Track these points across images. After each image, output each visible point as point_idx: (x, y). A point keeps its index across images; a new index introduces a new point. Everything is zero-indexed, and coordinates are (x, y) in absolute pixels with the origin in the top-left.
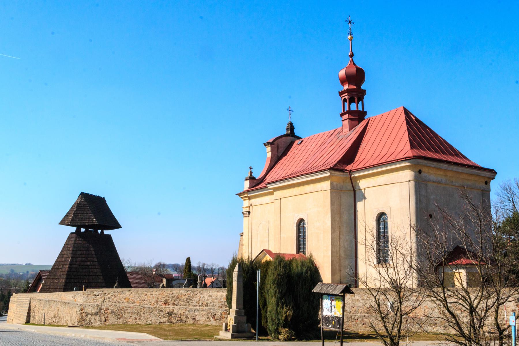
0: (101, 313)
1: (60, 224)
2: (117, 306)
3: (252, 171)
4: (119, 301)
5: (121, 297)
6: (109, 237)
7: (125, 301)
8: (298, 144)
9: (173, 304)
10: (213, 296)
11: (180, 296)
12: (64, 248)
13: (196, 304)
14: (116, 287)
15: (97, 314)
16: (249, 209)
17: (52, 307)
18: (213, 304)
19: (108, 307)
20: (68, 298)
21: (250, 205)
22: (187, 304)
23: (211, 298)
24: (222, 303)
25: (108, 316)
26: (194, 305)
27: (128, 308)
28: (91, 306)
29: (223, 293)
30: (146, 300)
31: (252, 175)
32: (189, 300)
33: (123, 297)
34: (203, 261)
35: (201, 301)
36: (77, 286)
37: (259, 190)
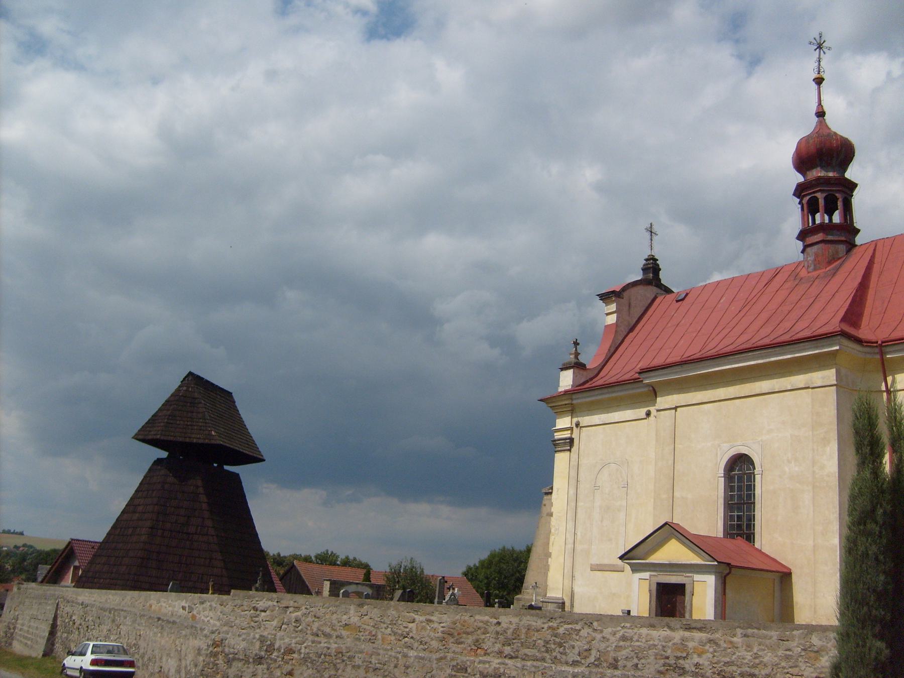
0: (271, 659)
1: (132, 438)
2: (322, 645)
3: (579, 351)
4: (328, 630)
5: (335, 622)
6: (236, 477)
7: (344, 633)
8: (677, 301)
9: (500, 653)
10: (636, 638)
11: (524, 631)
12: (137, 491)
13: (579, 658)
14: (257, 590)
15: (259, 660)
16: (572, 434)
17: (121, 627)
18: (635, 661)
19: (293, 645)
20: (170, 609)
21: (574, 426)
22: (548, 656)
23: (628, 643)
24: (667, 661)
25: (293, 670)
26: (570, 661)
27: (356, 652)
28: (244, 636)
29: (668, 632)
30: (411, 635)
31: (578, 359)
32: (553, 646)
33: (339, 622)
34: (269, 551)
35: (594, 653)
36: (176, 580)
37: (606, 390)
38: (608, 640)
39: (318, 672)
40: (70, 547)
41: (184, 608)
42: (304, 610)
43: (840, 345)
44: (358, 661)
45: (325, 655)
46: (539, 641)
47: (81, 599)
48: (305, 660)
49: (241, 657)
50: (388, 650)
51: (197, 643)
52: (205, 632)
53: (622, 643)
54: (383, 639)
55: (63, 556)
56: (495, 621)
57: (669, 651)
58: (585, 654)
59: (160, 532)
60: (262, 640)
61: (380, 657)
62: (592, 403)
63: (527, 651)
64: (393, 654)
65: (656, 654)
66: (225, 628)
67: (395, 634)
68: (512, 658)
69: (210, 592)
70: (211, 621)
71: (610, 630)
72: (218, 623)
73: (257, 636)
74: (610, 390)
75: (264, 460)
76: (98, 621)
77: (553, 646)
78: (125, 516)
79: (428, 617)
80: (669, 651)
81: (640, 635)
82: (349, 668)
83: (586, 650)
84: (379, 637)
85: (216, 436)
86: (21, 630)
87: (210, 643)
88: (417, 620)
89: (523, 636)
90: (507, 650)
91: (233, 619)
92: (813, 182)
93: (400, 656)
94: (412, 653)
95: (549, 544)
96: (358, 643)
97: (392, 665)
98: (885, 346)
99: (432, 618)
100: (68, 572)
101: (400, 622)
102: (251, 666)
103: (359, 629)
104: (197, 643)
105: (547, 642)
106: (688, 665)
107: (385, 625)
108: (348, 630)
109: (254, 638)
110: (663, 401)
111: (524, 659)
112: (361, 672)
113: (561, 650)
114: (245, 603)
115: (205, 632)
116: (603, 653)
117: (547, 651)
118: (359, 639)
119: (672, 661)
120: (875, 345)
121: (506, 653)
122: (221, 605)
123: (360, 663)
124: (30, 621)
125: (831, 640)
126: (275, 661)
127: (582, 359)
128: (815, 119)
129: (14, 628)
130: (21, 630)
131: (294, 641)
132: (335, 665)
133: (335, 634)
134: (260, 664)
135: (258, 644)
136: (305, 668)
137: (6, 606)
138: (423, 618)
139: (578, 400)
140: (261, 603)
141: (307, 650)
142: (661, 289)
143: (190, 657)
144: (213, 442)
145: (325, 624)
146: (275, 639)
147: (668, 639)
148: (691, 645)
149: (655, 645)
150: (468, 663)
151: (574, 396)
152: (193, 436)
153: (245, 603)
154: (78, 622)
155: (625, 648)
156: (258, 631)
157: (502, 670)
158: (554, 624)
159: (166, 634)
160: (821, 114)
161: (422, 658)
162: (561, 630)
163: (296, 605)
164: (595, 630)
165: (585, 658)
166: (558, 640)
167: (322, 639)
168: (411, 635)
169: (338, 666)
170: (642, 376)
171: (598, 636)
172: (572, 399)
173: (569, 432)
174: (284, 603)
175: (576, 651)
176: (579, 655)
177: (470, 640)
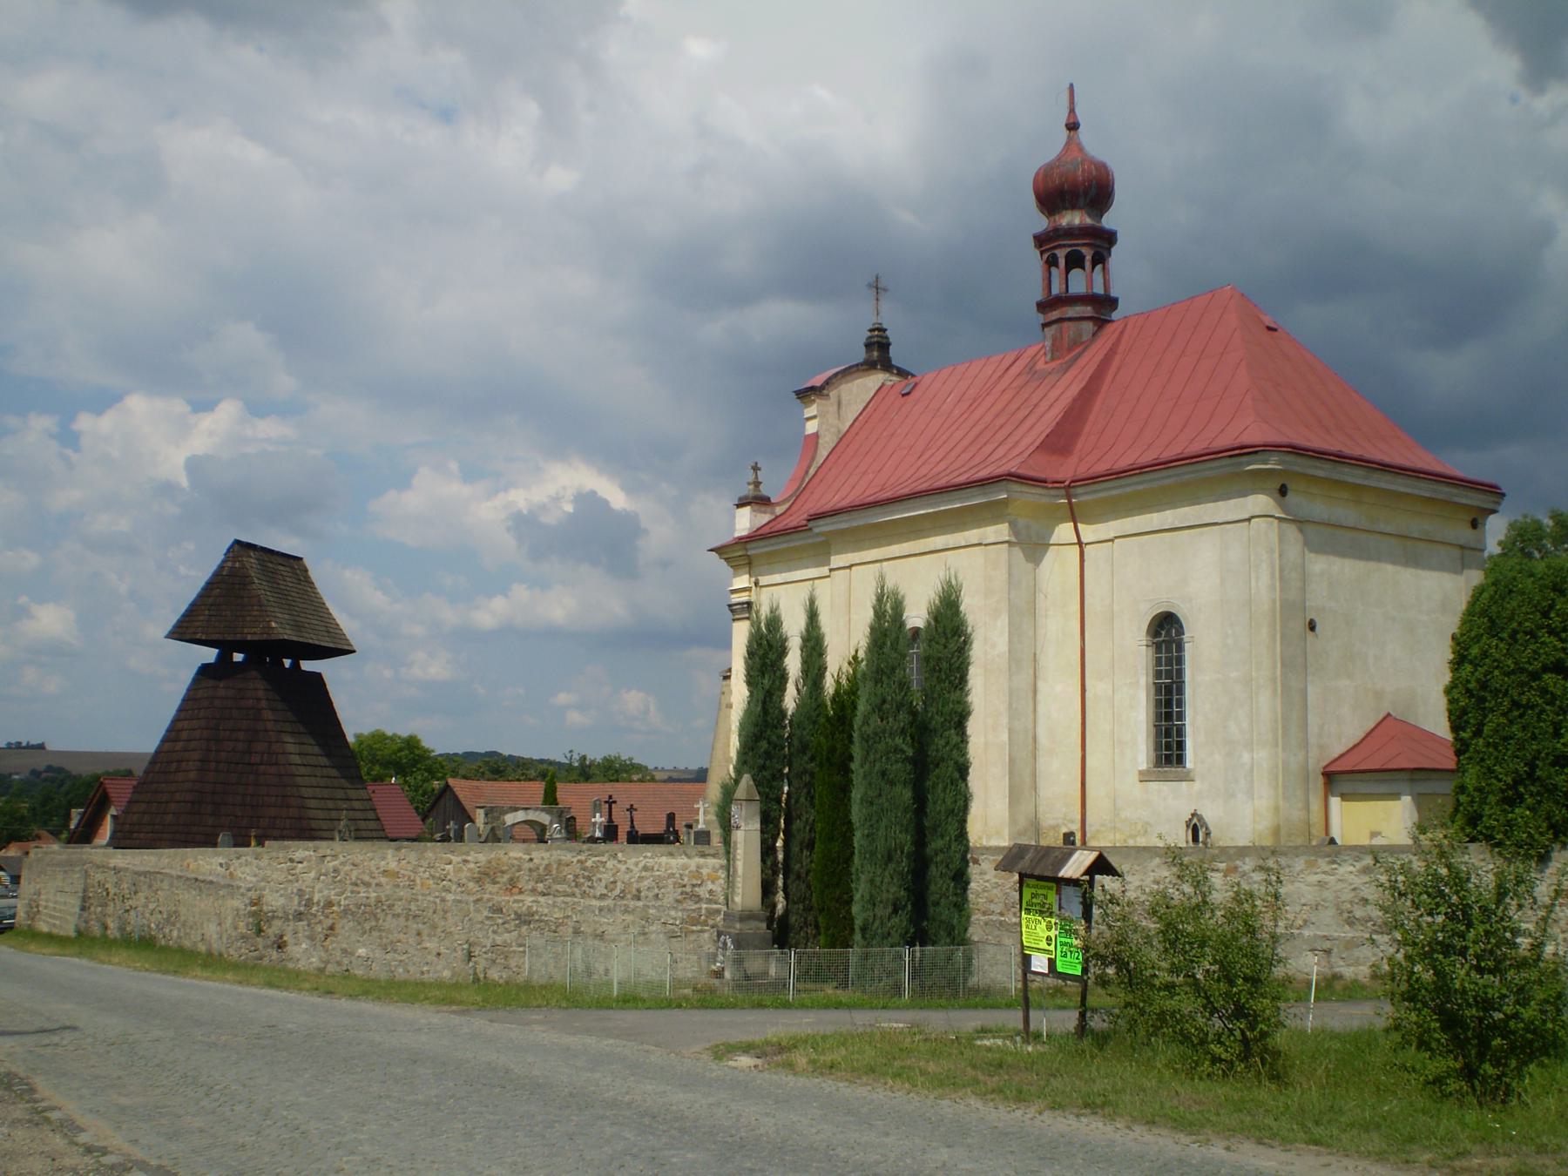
0: (312, 914)
2: (362, 895)
4: (366, 878)
5: (373, 869)
6: (317, 678)
7: (383, 880)
8: (903, 395)
9: (534, 890)
11: (555, 866)
13: (605, 892)
15: (299, 916)
17: (159, 892)
18: (656, 891)
23: (648, 874)
25: (334, 924)
28: (282, 892)
29: (684, 860)
30: (449, 877)
32: (582, 880)
33: (378, 868)
38: (632, 871)
39: (359, 924)
40: (100, 791)
41: (221, 865)
42: (341, 858)
43: (1007, 491)
44: (398, 910)
45: (365, 906)
46: (569, 876)
47: (113, 862)
48: (346, 911)
49: (280, 915)
50: (426, 895)
51: (237, 903)
52: (242, 890)
53: (644, 874)
54: (422, 884)
55: (94, 802)
56: (527, 857)
57: (686, 879)
58: (612, 886)
59: (213, 765)
60: (301, 893)
61: (419, 903)
62: (770, 554)
63: (559, 887)
64: (432, 899)
65: (675, 883)
66: (263, 884)
67: (433, 877)
68: (544, 895)
69: (253, 843)
70: (248, 878)
71: (633, 860)
72: (254, 879)
73: (295, 891)
74: (788, 538)
75: (354, 651)
76: (133, 888)
77: (582, 880)
78: (167, 746)
79: (464, 857)
80: (686, 879)
81: (660, 865)
82: (390, 917)
83: (612, 882)
84: (418, 881)
85: (281, 628)
86: (46, 907)
87: (247, 901)
88: (454, 861)
89: (554, 872)
90: (540, 887)
91: (269, 872)
92: (1051, 234)
93: (438, 901)
94: (450, 897)
95: (729, 746)
96: (397, 890)
97: (431, 911)
98: (1074, 487)
99: (469, 858)
100: (104, 823)
101: (437, 865)
102: (291, 923)
103: (396, 875)
104: (237, 903)
105: (576, 876)
106: (702, 892)
107: (423, 869)
108: (386, 876)
109: (292, 893)
110: (837, 560)
111: (555, 896)
112: (402, 920)
113: (590, 884)
114: (281, 855)
115: (242, 890)
116: (628, 884)
117: (576, 886)
118: (398, 886)
119: (688, 889)
120: (1062, 485)
121: (539, 890)
122: (256, 859)
123: (400, 911)
124: (55, 895)
125: (529, 854)
126: (315, 916)
127: (764, 490)
128: (1064, 133)
129: (37, 906)
130: (46, 907)
131: (333, 892)
132: (375, 916)
133: (374, 882)
134: (300, 920)
135: (296, 899)
136: (346, 921)
137: (23, 877)
138: (459, 859)
139: (754, 550)
140: (297, 854)
141: (347, 902)
142: (892, 373)
143: (229, 920)
144: (273, 637)
145: (364, 872)
146: (313, 892)
147: (685, 867)
148: (705, 871)
149: (673, 874)
150: (503, 903)
151: (749, 546)
152: (246, 631)
153: (281, 855)
154: (112, 891)
155: (647, 879)
156: (296, 884)
157: (534, 909)
158: (582, 857)
159: (204, 896)
160: (1073, 126)
161: (459, 901)
162: (589, 864)
163: (333, 852)
164: (620, 862)
165: (611, 890)
166: (586, 874)
167: (362, 889)
168: (449, 877)
169: (378, 916)
170: (811, 524)
171: (623, 867)
172: (746, 550)
173: (747, 593)
174: (321, 852)
175: (603, 883)
176: (606, 888)
177: (506, 878)
